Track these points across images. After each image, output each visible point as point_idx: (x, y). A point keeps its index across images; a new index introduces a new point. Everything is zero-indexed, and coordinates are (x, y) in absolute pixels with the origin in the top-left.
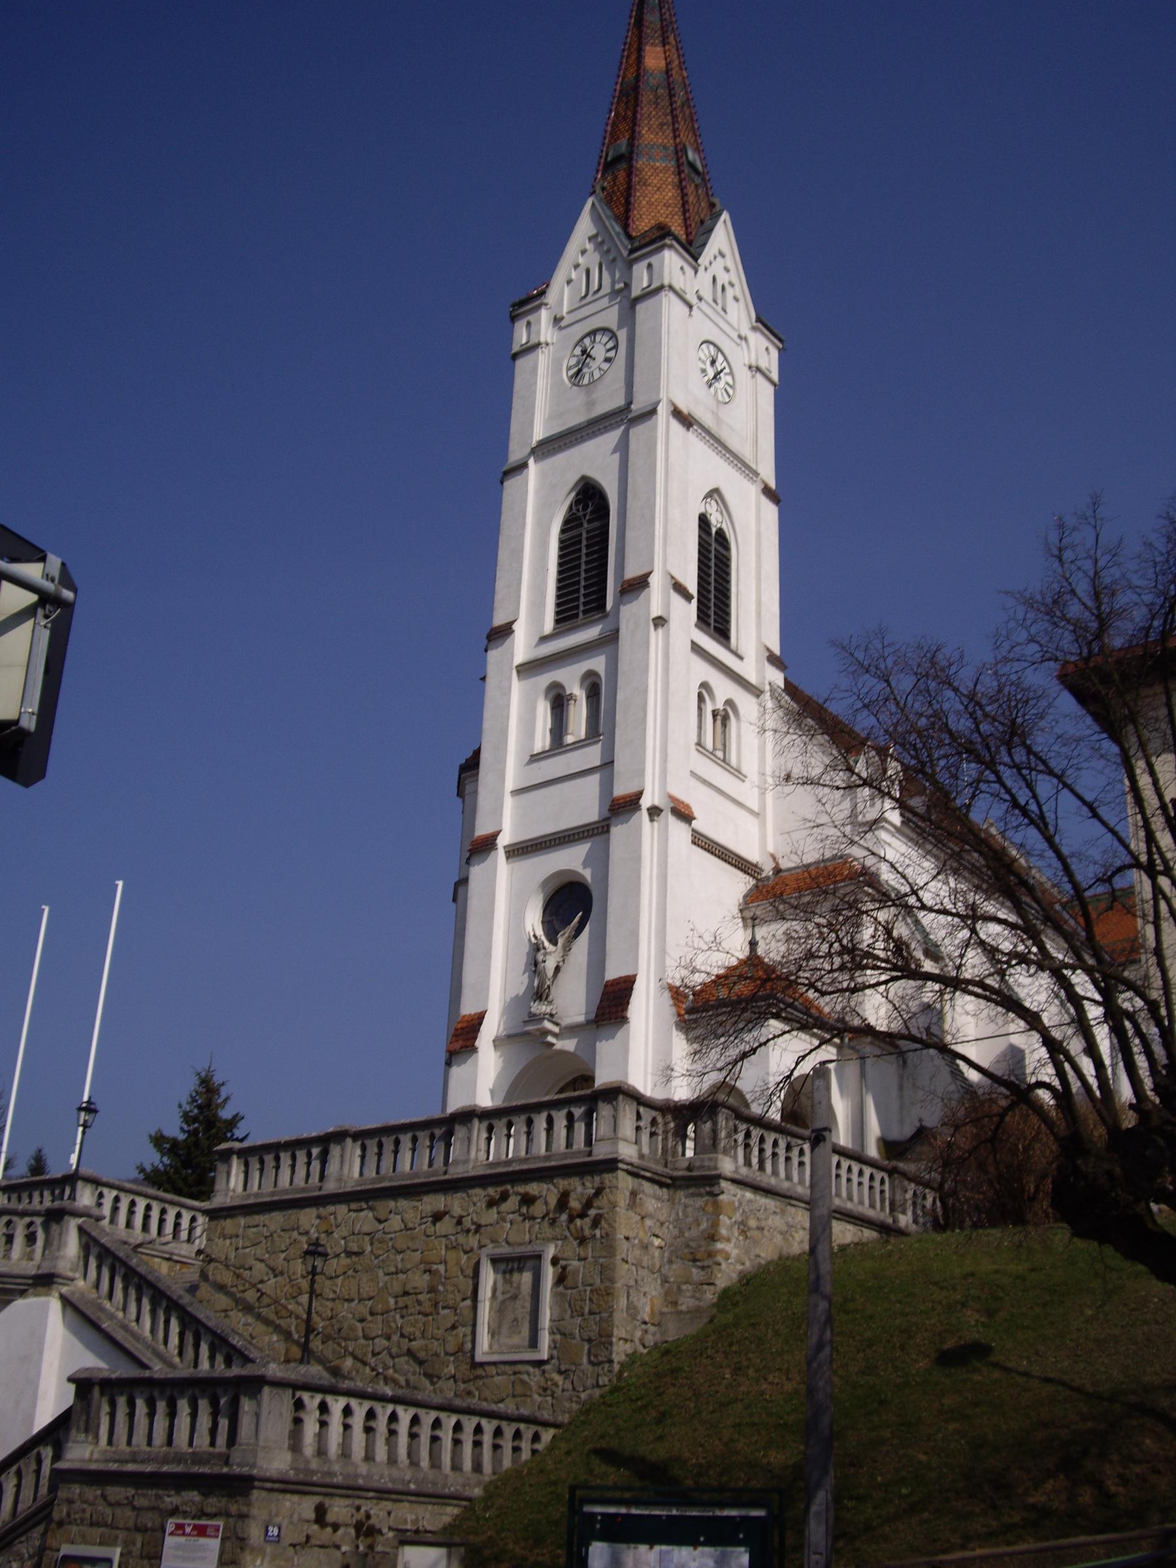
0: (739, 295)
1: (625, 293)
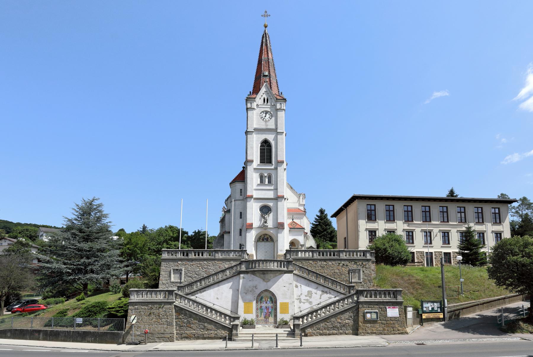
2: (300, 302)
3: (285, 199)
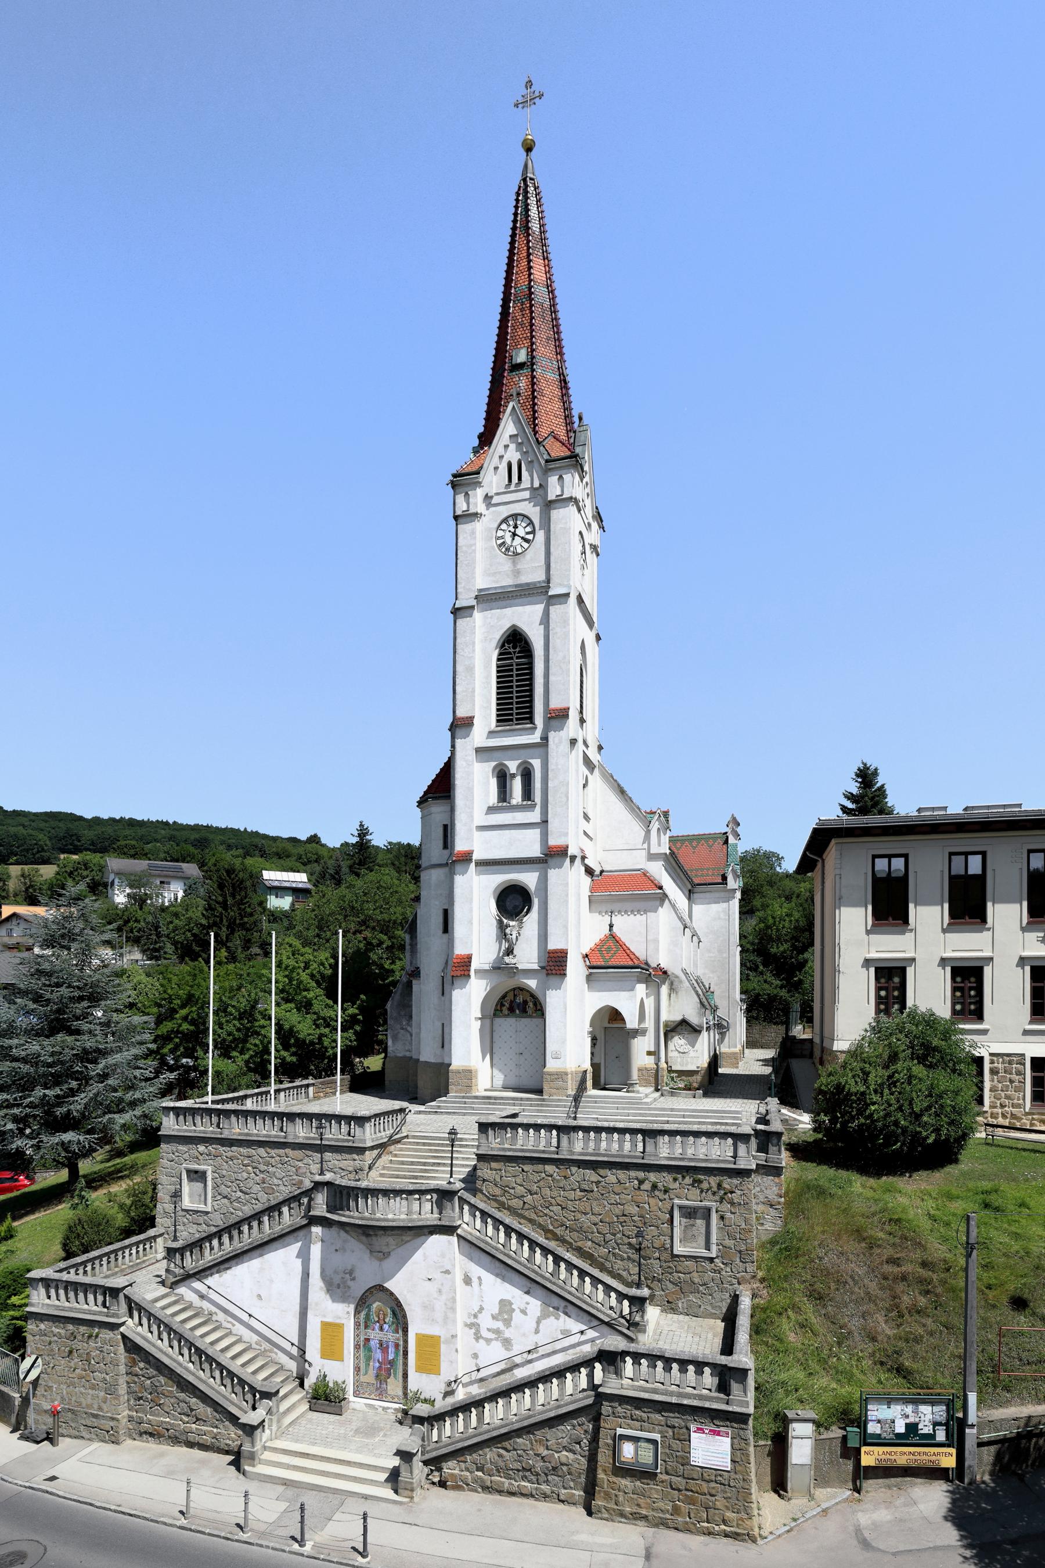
1: (541, 492)
2: (478, 1337)
3: (573, 859)
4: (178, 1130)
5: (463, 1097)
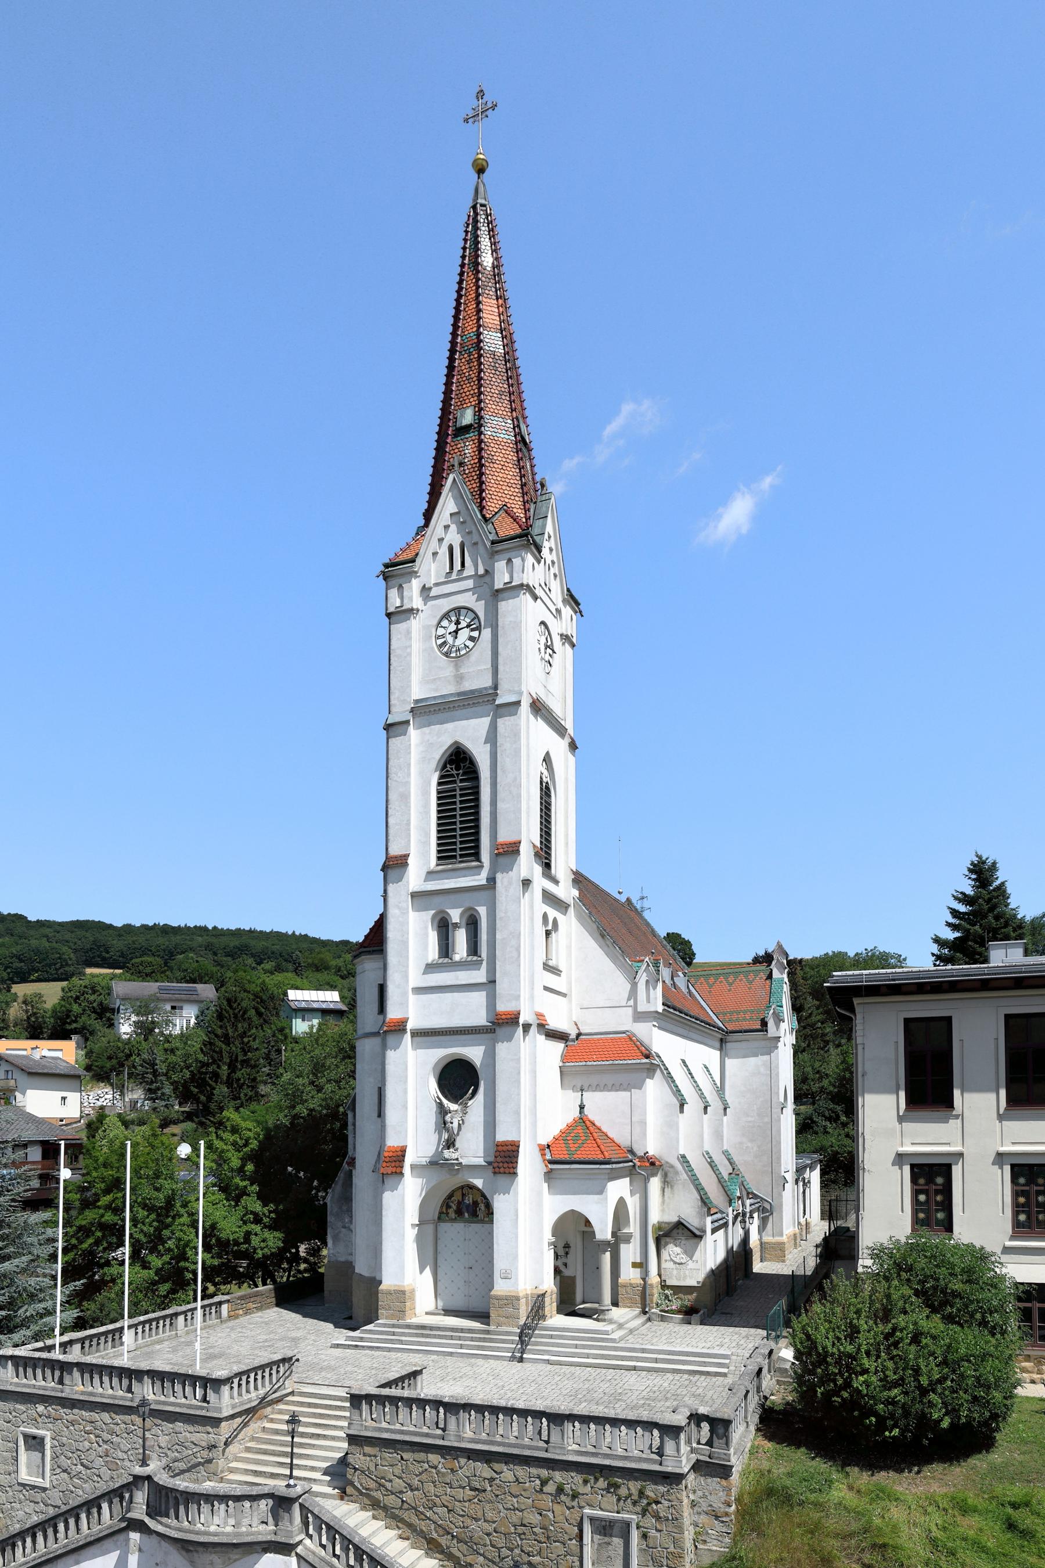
0: (554, 547)
1: (487, 579)
3: (527, 1027)
4: (17, 1385)
5: (393, 1326)
